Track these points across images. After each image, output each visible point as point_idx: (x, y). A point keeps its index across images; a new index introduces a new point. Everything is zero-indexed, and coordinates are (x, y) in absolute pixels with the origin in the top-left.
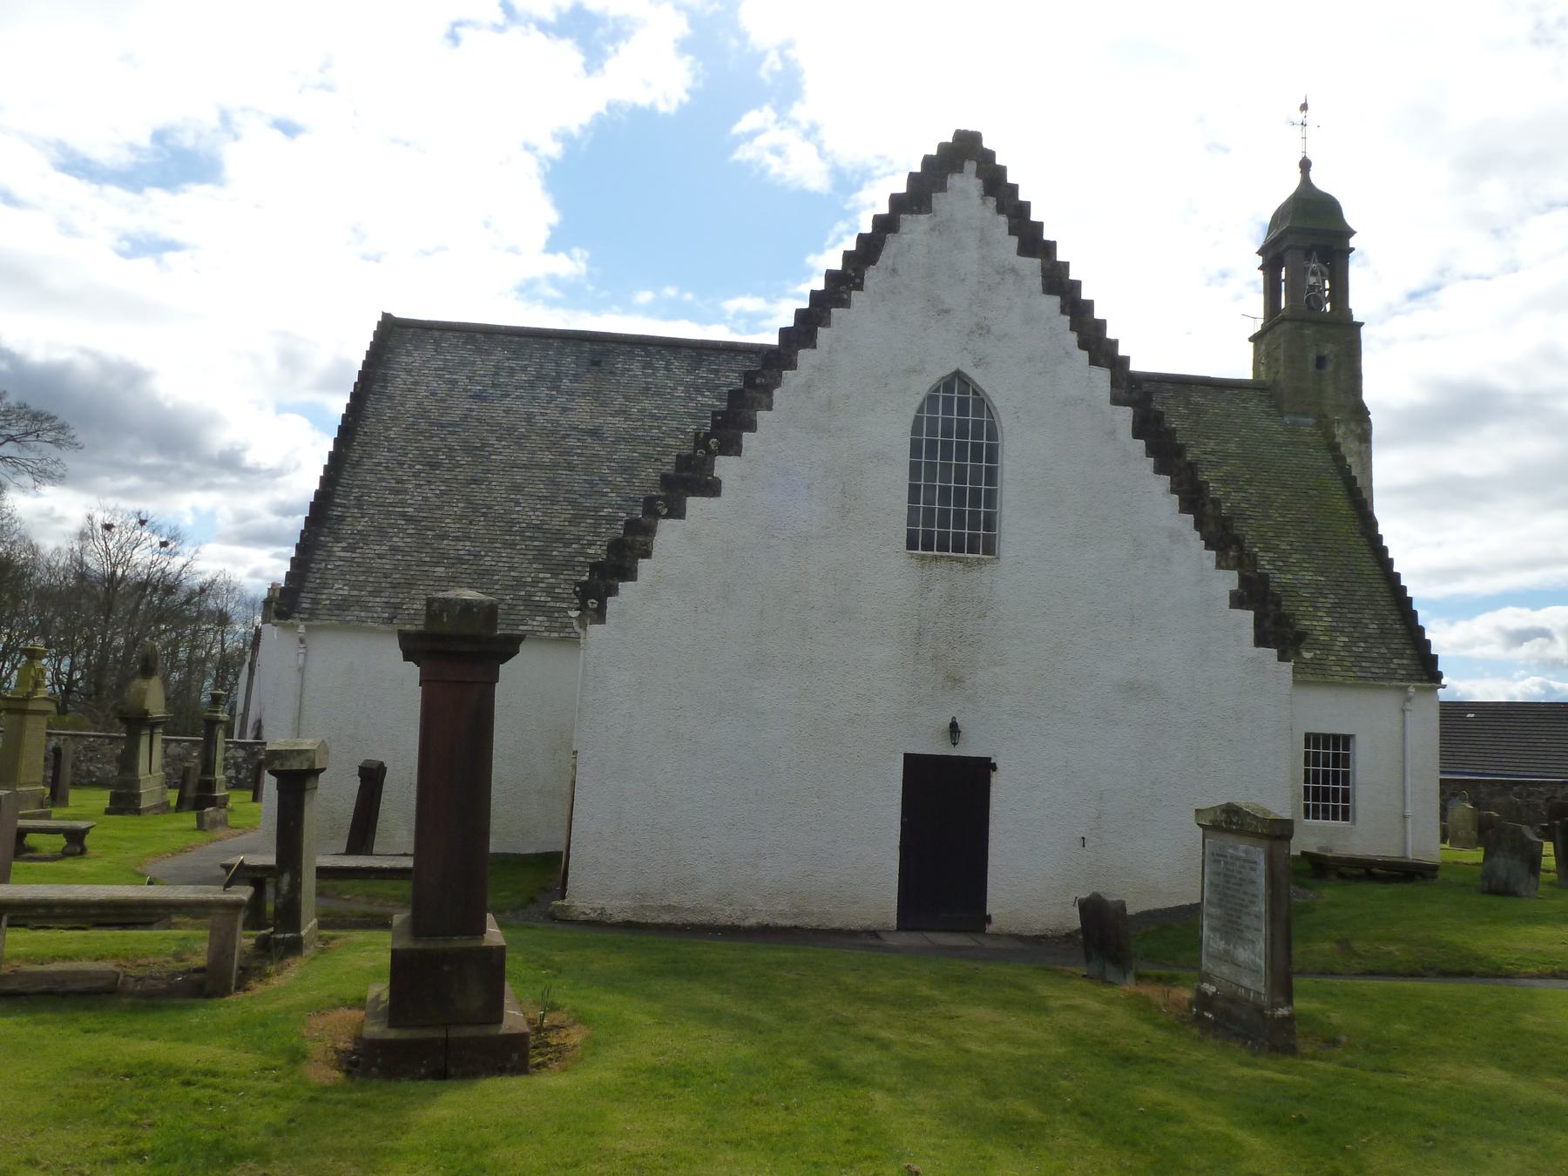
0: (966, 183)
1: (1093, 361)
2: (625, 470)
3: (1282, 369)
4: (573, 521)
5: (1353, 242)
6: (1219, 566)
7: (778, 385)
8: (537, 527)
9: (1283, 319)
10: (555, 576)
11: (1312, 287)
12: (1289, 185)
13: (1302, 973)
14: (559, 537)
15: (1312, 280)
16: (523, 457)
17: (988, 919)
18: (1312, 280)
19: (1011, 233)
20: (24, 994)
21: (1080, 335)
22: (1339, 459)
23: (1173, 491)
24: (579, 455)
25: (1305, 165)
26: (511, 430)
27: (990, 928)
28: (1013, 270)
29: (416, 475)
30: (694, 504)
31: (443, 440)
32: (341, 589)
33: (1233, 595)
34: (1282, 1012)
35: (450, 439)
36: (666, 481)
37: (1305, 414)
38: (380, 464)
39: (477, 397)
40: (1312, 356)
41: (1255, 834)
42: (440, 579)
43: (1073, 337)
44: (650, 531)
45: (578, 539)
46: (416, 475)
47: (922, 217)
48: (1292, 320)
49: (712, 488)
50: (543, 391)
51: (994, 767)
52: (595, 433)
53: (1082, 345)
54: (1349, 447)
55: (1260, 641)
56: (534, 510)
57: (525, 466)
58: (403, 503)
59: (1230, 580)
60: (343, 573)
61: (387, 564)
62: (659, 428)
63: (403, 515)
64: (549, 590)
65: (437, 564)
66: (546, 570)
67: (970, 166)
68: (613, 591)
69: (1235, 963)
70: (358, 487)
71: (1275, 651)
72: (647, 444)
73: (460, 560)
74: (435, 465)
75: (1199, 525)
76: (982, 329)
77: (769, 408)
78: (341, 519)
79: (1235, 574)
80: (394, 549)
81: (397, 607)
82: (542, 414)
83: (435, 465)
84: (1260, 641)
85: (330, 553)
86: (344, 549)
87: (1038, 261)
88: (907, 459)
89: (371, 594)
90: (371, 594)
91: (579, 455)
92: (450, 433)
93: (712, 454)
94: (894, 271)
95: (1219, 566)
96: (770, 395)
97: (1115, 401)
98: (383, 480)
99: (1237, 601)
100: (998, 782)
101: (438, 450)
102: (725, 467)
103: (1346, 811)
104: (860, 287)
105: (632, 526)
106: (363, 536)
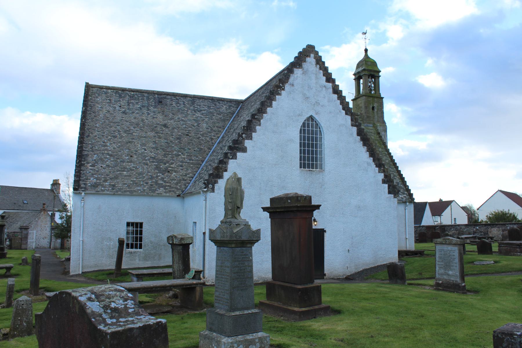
0: (311, 60)
1: (346, 114)
2: (178, 138)
3: (363, 110)
4: (165, 155)
5: (380, 74)
6: (379, 172)
7: (262, 118)
8: (154, 158)
9: (363, 96)
10: (163, 174)
11: (370, 86)
12: (362, 56)
13: (467, 275)
14: (160, 161)
15: (370, 84)
16: (144, 134)
17: (325, 275)
18: (370, 84)
19: (324, 75)
20: (515, 271)
21: (343, 106)
22: (380, 137)
23: (367, 151)
24: (162, 133)
25: (366, 50)
26: (138, 124)
27: (325, 277)
28: (325, 86)
29: (109, 140)
30: (239, 154)
31: (116, 128)
32: (93, 180)
33: (383, 180)
34: (463, 284)
35: (118, 128)
36: (230, 148)
37: (370, 123)
38: (96, 136)
39: (124, 112)
40: (371, 106)
41: (455, 244)
42: (126, 176)
43: (341, 106)
44: (226, 163)
45: (168, 162)
46: (109, 140)
47: (300, 70)
48: (365, 96)
49: (244, 150)
50: (145, 111)
51: (325, 231)
52: (165, 126)
53: (343, 109)
54: (382, 133)
55: (389, 193)
56: (151, 152)
57: (145, 137)
58: (107, 150)
59: (381, 176)
60: (93, 174)
61: (107, 171)
62: (186, 124)
63: (108, 154)
64: (162, 179)
65: (124, 171)
66: (160, 173)
67: (312, 55)
68: (216, 182)
69: (448, 275)
70: (90, 144)
71: (393, 195)
72: (183, 130)
73: (131, 170)
74: (115, 137)
75: (374, 161)
76: (317, 103)
77: (260, 125)
78: (87, 155)
79: (383, 174)
80: (108, 166)
81: (114, 186)
82: (147, 119)
83: (115, 137)
84: (389, 193)
85: (87, 168)
86: (91, 166)
87: (331, 84)
88: (299, 141)
89: (104, 181)
90: (104, 181)
91: (162, 133)
92: (117, 125)
93: (244, 139)
94: (293, 85)
95: (379, 172)
96: (260, 121)
97: (352, 125)
98: (99, 142)
99: (384, 182)
100: (326, 235)
101: (115, 131)
102: (247, 143)
103: (141, 245)
104: (284, 89)
105: (221, 162)
106: (96, 162)
